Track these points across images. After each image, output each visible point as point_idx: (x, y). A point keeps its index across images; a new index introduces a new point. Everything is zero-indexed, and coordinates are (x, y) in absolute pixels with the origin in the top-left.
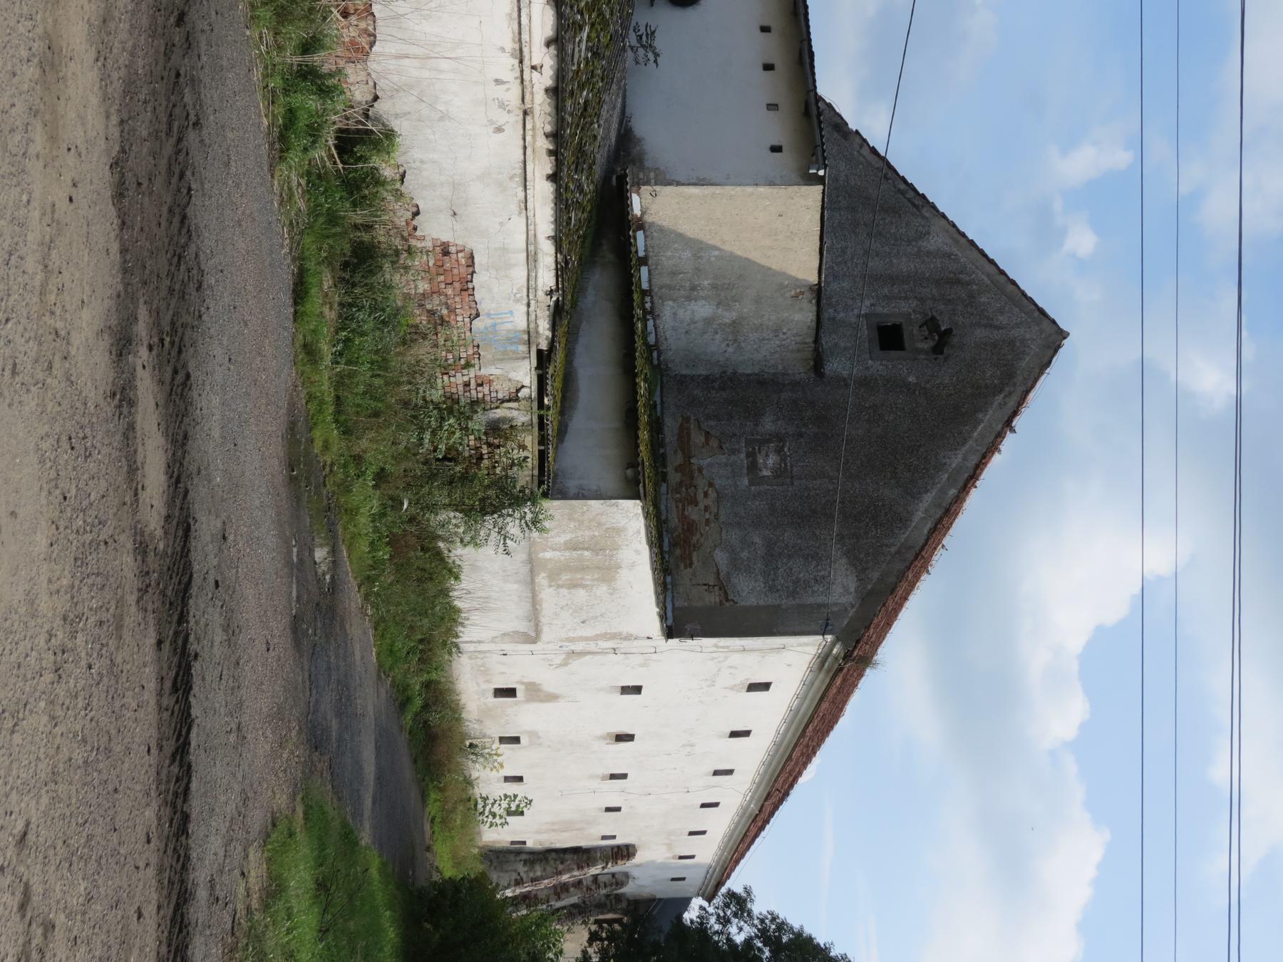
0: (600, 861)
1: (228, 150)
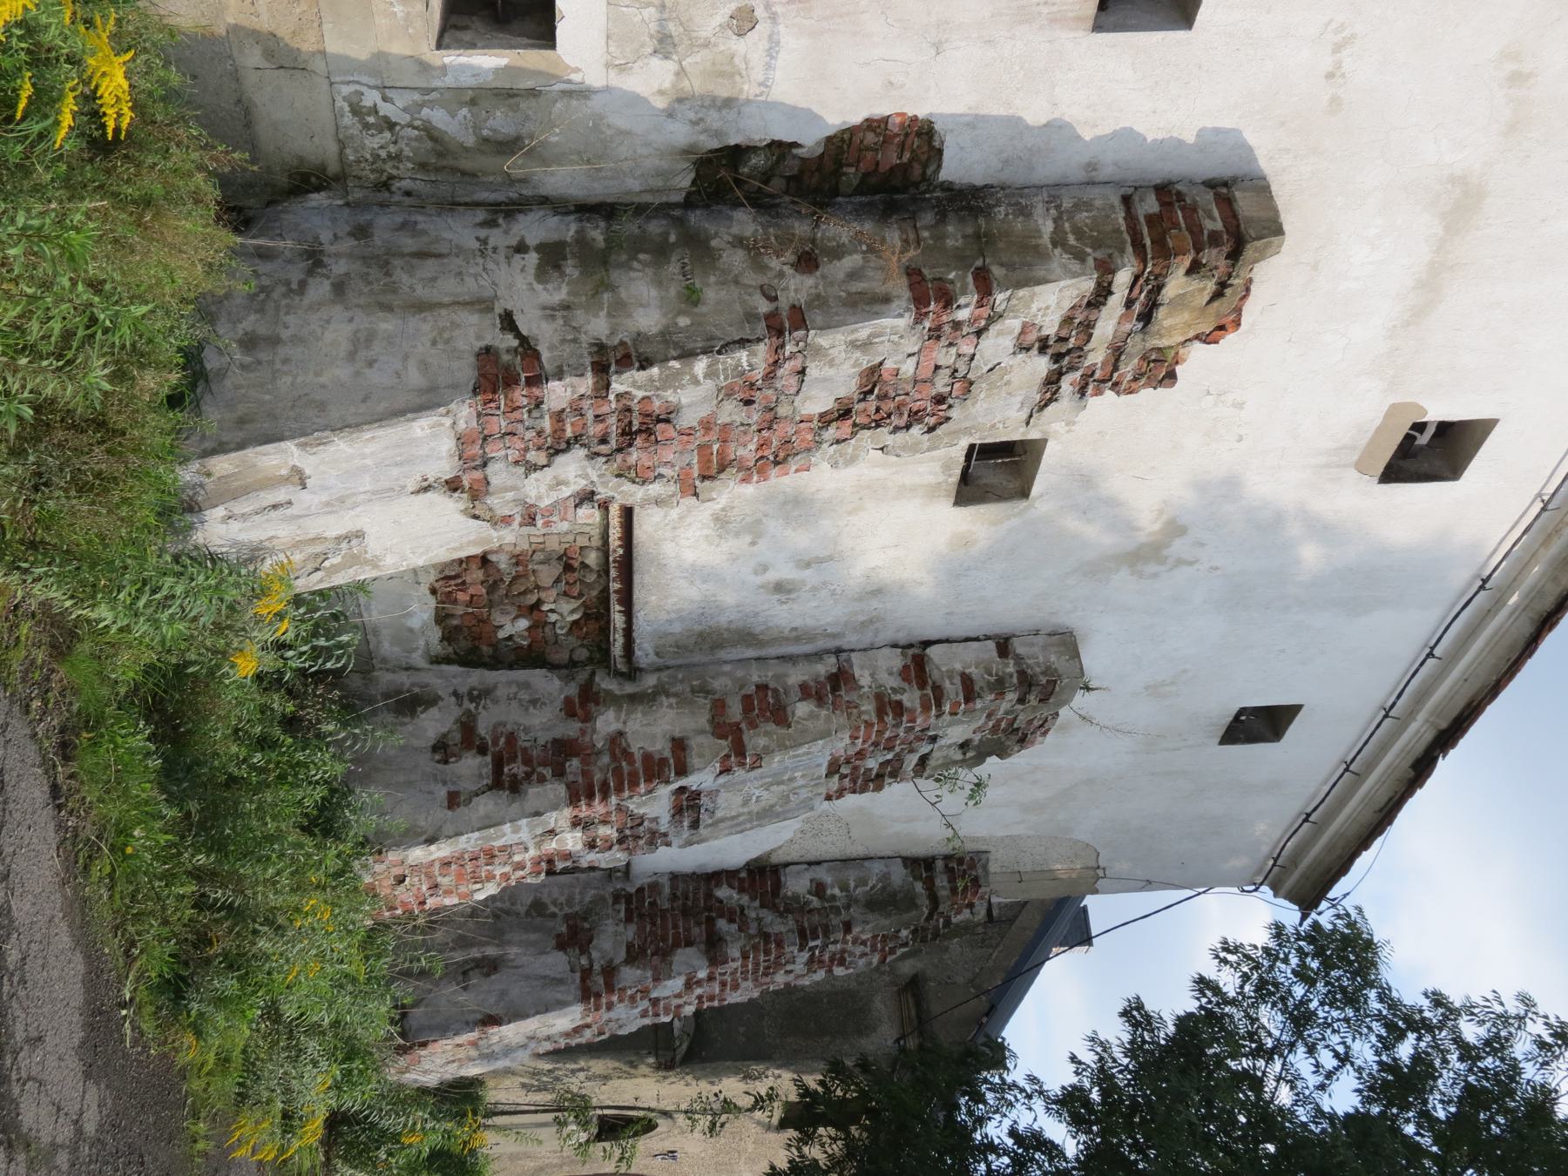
0: (1059, 258)
1: (141, 1156)
